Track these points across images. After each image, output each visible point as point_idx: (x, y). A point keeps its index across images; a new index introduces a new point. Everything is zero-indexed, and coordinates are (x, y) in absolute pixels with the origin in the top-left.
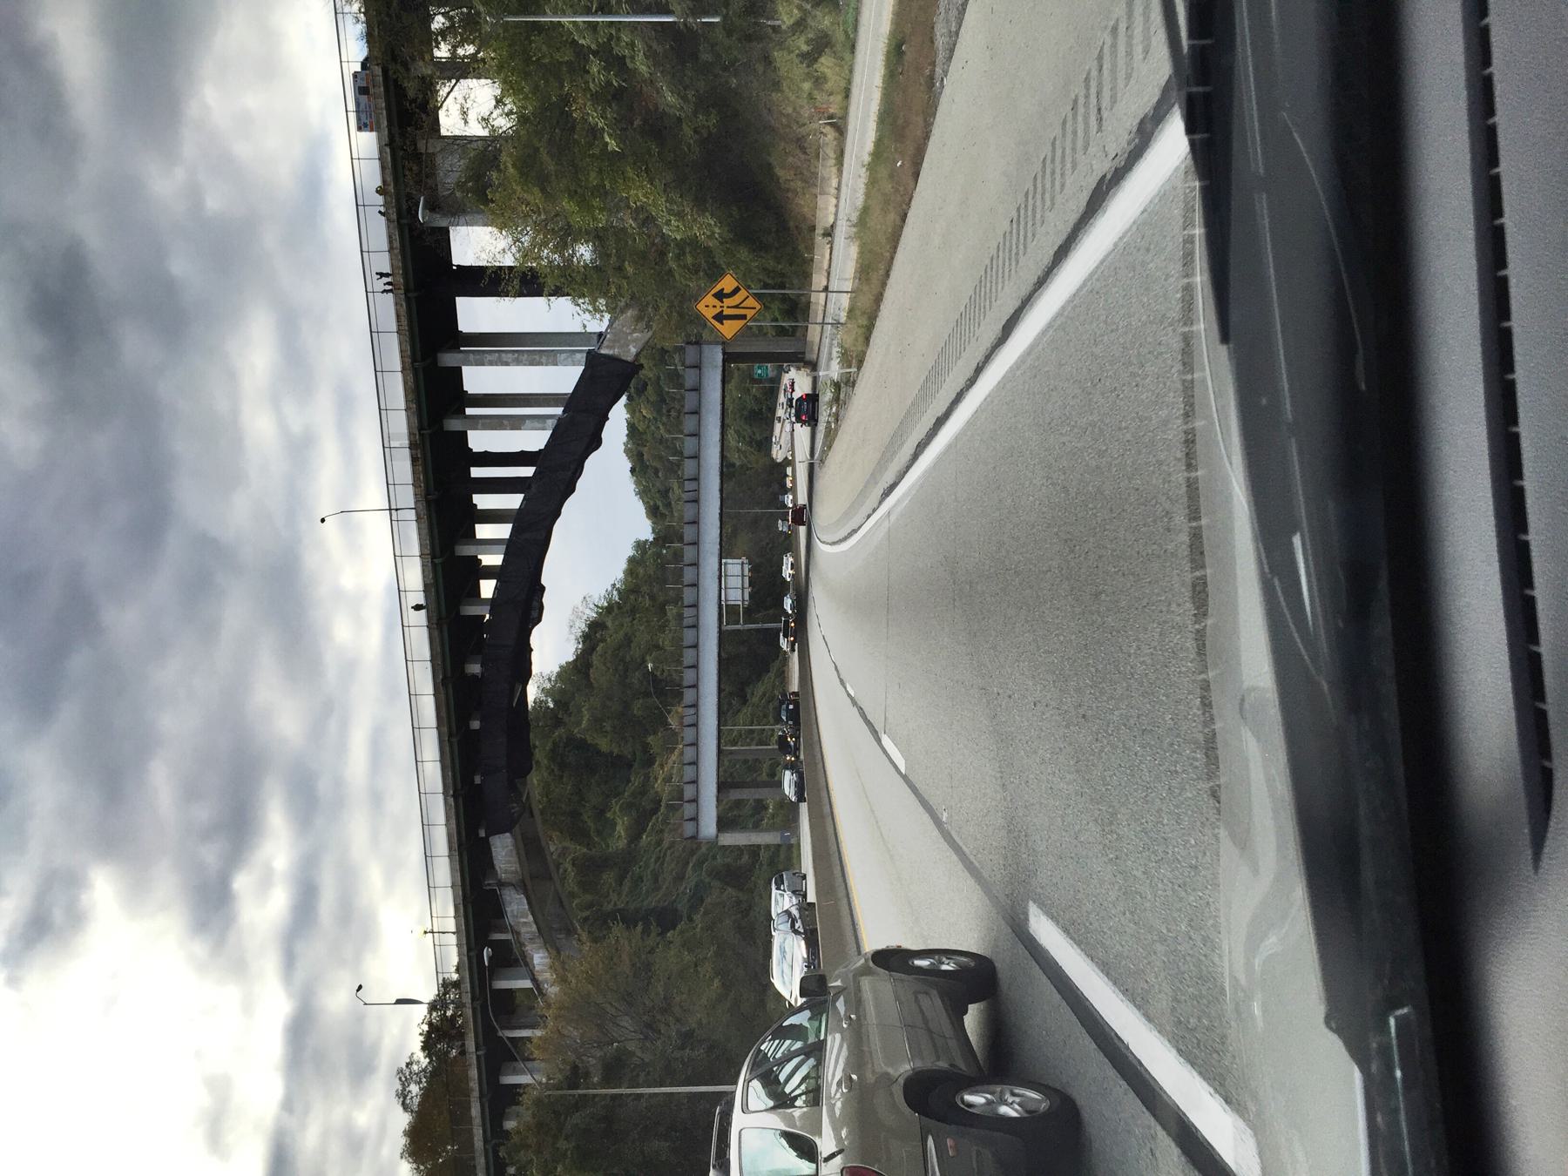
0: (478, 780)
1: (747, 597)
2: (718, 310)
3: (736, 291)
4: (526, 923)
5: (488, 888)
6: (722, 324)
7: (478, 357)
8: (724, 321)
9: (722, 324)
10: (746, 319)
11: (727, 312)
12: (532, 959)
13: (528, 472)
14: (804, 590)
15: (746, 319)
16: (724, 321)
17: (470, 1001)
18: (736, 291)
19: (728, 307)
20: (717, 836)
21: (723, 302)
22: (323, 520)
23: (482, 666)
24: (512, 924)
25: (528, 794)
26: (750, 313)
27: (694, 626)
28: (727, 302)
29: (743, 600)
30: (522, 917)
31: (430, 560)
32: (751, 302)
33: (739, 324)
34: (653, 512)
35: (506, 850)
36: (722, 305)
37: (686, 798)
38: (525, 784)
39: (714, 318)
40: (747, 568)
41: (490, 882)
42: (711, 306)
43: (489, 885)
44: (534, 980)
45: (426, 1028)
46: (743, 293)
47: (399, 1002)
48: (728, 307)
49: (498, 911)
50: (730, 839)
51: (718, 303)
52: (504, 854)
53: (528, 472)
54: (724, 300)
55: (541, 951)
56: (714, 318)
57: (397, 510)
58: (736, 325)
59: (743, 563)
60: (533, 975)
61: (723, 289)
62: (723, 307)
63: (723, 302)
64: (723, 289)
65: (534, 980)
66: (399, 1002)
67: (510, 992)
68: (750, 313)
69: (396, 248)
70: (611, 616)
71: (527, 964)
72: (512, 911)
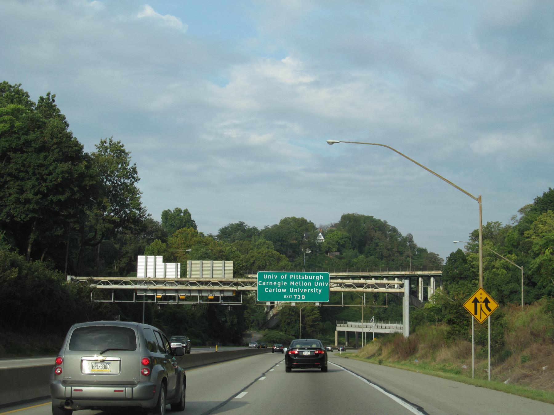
2: (479, 300)
3: (489, 310)
6: (473, 302)
9: (473, 302)
11: (479, 305)
18: (489, 310)
21: (483, 302)
26: (478, 317)
28: (483, 305)
32: (484, 317)
42: (481, 296)
48: (481, 305)
50: (336, 333)
51: (483, 300)
61: (489, 303)
62: (481, 302)
63: (483, 302)
64: (489, 303)
68: (478, 317)
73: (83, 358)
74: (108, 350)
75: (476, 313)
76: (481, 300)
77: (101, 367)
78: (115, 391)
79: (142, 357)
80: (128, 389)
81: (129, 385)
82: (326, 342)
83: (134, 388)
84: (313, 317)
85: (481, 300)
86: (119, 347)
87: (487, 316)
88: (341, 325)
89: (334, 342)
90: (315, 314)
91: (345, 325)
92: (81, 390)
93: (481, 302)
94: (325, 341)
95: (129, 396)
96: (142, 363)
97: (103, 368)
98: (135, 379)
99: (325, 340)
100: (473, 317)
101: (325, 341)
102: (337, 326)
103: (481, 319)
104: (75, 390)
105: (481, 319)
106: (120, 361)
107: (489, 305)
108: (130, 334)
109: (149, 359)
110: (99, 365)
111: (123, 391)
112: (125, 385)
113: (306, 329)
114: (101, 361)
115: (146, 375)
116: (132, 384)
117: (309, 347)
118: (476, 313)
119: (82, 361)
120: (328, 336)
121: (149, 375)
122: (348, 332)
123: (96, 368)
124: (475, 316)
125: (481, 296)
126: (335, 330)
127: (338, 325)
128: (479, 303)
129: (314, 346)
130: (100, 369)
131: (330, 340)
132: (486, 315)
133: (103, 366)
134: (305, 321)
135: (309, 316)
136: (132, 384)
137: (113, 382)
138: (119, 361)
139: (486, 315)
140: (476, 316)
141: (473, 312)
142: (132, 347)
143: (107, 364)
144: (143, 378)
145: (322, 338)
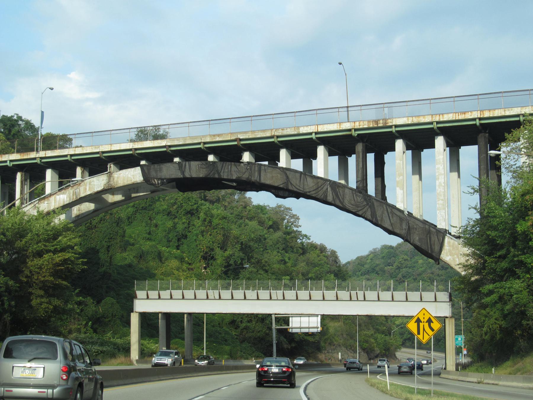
0: (177, 160)
1: (294, 331)
2: (422, 320)
3: (432, 330)
4: (86, 189)
5: (108, 166)
6: (415, 322)
7: (441, 161)
8: (416, 323)
9: (415, 322)
10: (418, 334)
11: (421, 325)
12: (63, 193)
13: (371, 190)
14: (19, 200)
15: (418, 334)
16: (416, 323)
17: (40, 156)
18: (432, 330)
19: (424, 325)
20: (136, 312)
21: (426, 322)
22: (340, 64)
23: (247, 162)
24: (86, 181)
25: (167, 190)
26: (420, 336)
27: (271, 298)
28: (426, 325)
29: (292, 328)
30: (90, 188)
31: (314, 131)
32: (426, 338)
33: (415, 331)
34: (360, 261)
35: (132, 177)
36: (425, 322)
37: (161, 292)
38: (173, 187)
39: (418, 318)
40: (315, 330)
41: (112, 167)
42: (424, 316)
43: (110, 167)
44: (50, 195)
45: (15, 118)
46: (431, 333)
47: (42, 112)
48: (424, 325)
49: (93, 173)
50: (135, 319)
51: (426, 320)
52: (129, 176)
53: (371, 190)
54: (427, 323)
55: (68, 199)
56: (418, 318)
57: (348, 111)
58: (414, 330)
59: (318, 328)
60: (53, 195)
61: (433, 322)
62: (424, 322)
63: (426, 322)
64: (433, 322)
65: (50, 195)
66: (42, 112)
67: (43, 178)
68: (420, 336)
69: (505, 113)
70: (283, 234)
71: (59, 190)
72: (93, 181)
73: (14, 365)
74: (35, 359)
75: (419, 333)
76: (424, 320)
77: (28, 373)
78: (39, 392)
79: (62, 365)
80: (50, 391)
81: (50, 388)
82: (105, 349)
83: (55, 391)
84: (58, 258)
85: (424, 320)
86: (48, 357)
87: (429, 337)
88: (150, 293)
89: (127, 350)
90: (63, 250)
91: (161, 292)
92: (11, 391)
93: (424, 322)
94: (100, 348)
95: (50, 396)
96: (62, 370)
97: (30, 373)
98: (56, 382)
99: (102, 345)
100: (416, 337)
101: (100, 348)
102: (136, 297)
103: (423, 339)
104: (7, 391)
105: (423, 339)
106: (44, 368)
107: (432, 325)
108: (53, 345)
109: (67, 366)
110: (27, 371)
111: (44, 392)
112: (48, 388)
113: (31, 300)
114: (28, 368)
115: (64, 380)
116: (53, 387)
117: (278, 364)
118: (419, 333)
119: (13, 367)
120: (109, 335)
121: (67, 380)
122: (168, 316)
123: (24, 373)
124: (418, 336)
125: (424, 316)
126: (132, 310)
127: (140, 294)
128: (422, 322)
129: (283, 364)
130: (27, 374)
131: (115, 344)
132: (429, 335)
133: (30, 371)
134: (27, 272)
135: (39, 254)
136: (53, 387)
137: (39, 384)
138: (43, 368)
139: (429, 335)
140: (418, 336)
141: (416, 333)
142: (54, 357)
143: (33, 370)
144: (63, 382)
145: (92, 338)
